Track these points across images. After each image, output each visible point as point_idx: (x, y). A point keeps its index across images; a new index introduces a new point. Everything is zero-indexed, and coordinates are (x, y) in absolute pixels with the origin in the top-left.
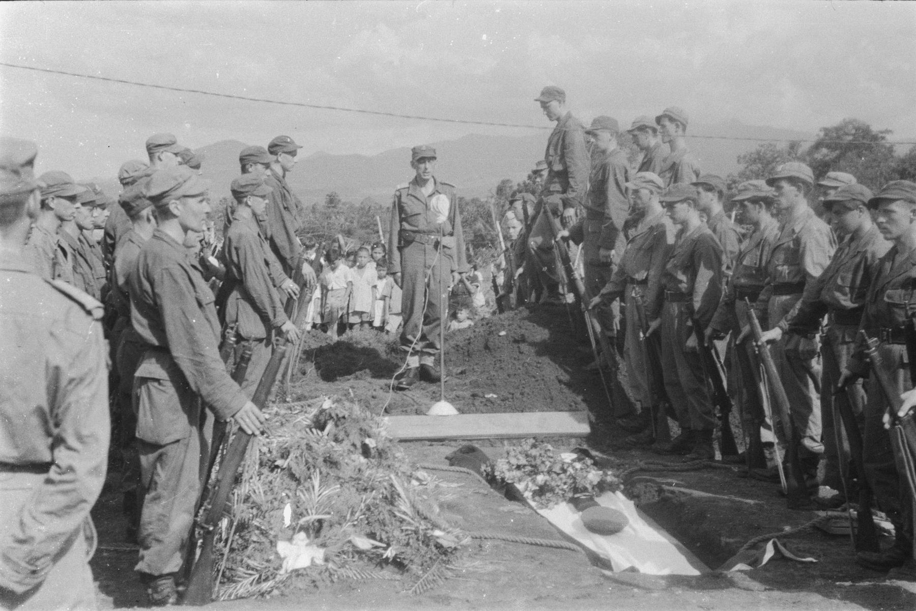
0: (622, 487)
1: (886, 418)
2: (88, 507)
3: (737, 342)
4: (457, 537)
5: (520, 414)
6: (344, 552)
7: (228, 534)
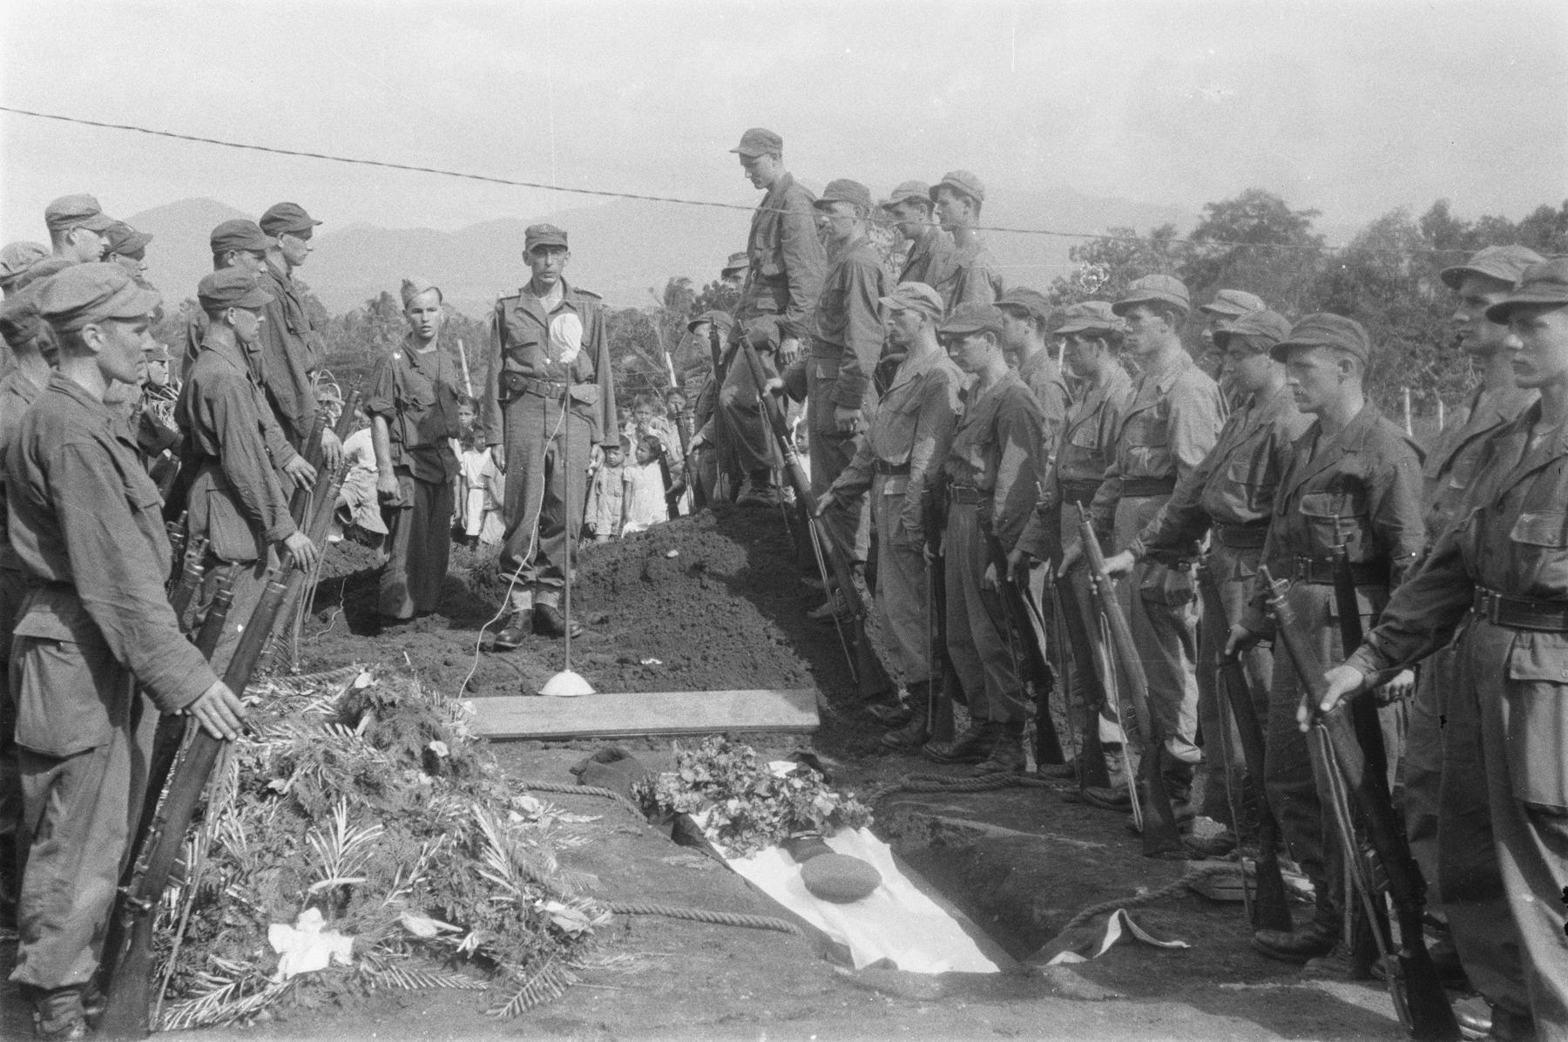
0: (871, 819)
1: (1302, 713)
4: (587, 912)
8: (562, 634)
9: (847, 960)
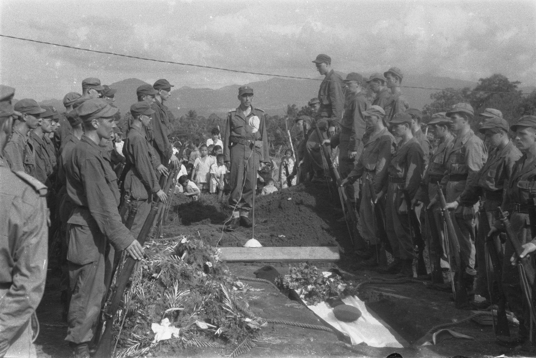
0: (358, 293)
2: (32, 311)
3: (428, 208)
4: (259, 322)
5: (299, 247)
6: (191, 331)
7: (122, 318)
8: (251, 226)
9: (349, 342)
